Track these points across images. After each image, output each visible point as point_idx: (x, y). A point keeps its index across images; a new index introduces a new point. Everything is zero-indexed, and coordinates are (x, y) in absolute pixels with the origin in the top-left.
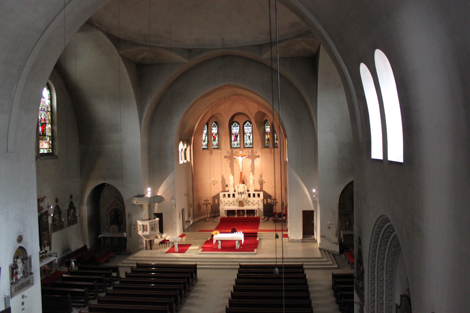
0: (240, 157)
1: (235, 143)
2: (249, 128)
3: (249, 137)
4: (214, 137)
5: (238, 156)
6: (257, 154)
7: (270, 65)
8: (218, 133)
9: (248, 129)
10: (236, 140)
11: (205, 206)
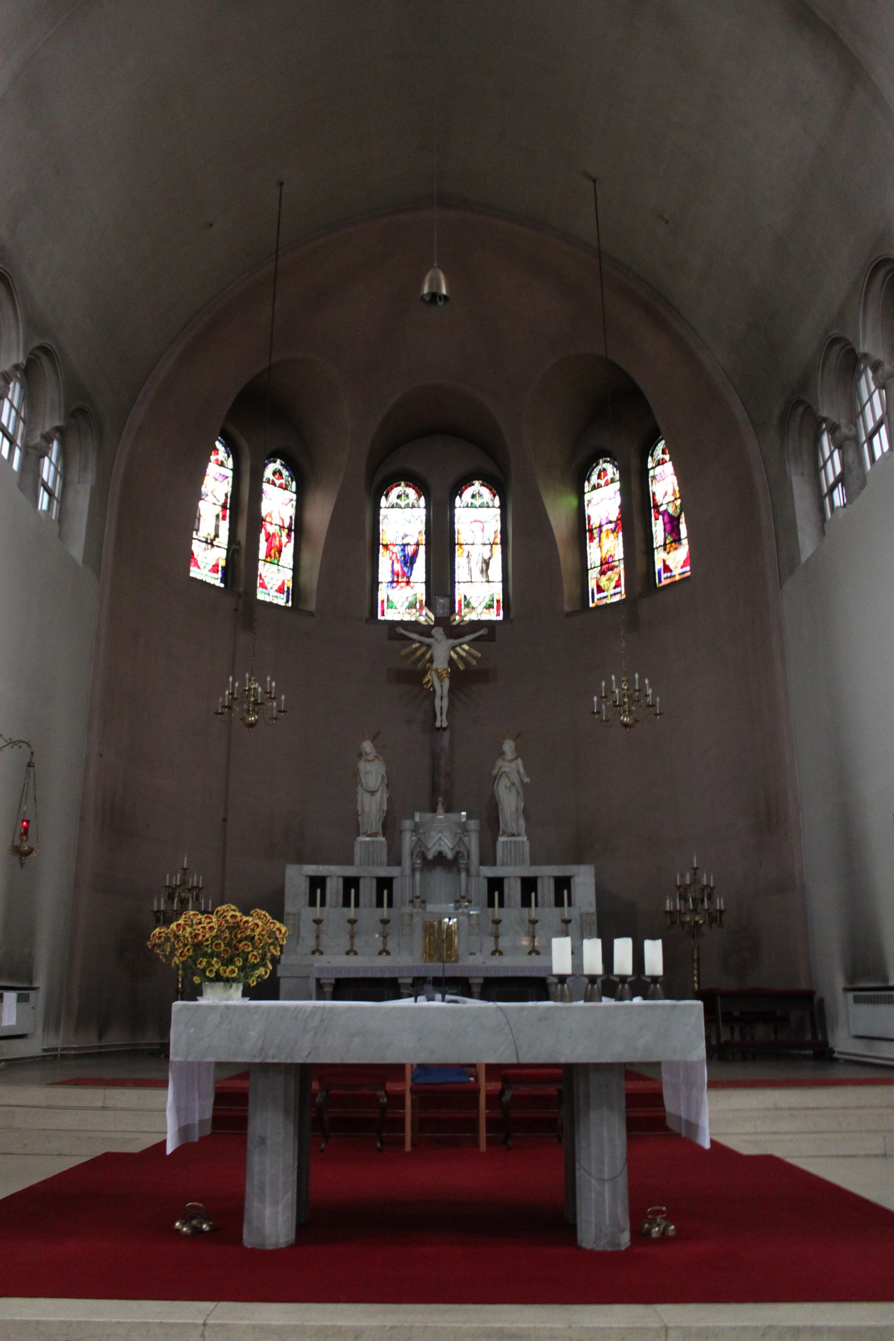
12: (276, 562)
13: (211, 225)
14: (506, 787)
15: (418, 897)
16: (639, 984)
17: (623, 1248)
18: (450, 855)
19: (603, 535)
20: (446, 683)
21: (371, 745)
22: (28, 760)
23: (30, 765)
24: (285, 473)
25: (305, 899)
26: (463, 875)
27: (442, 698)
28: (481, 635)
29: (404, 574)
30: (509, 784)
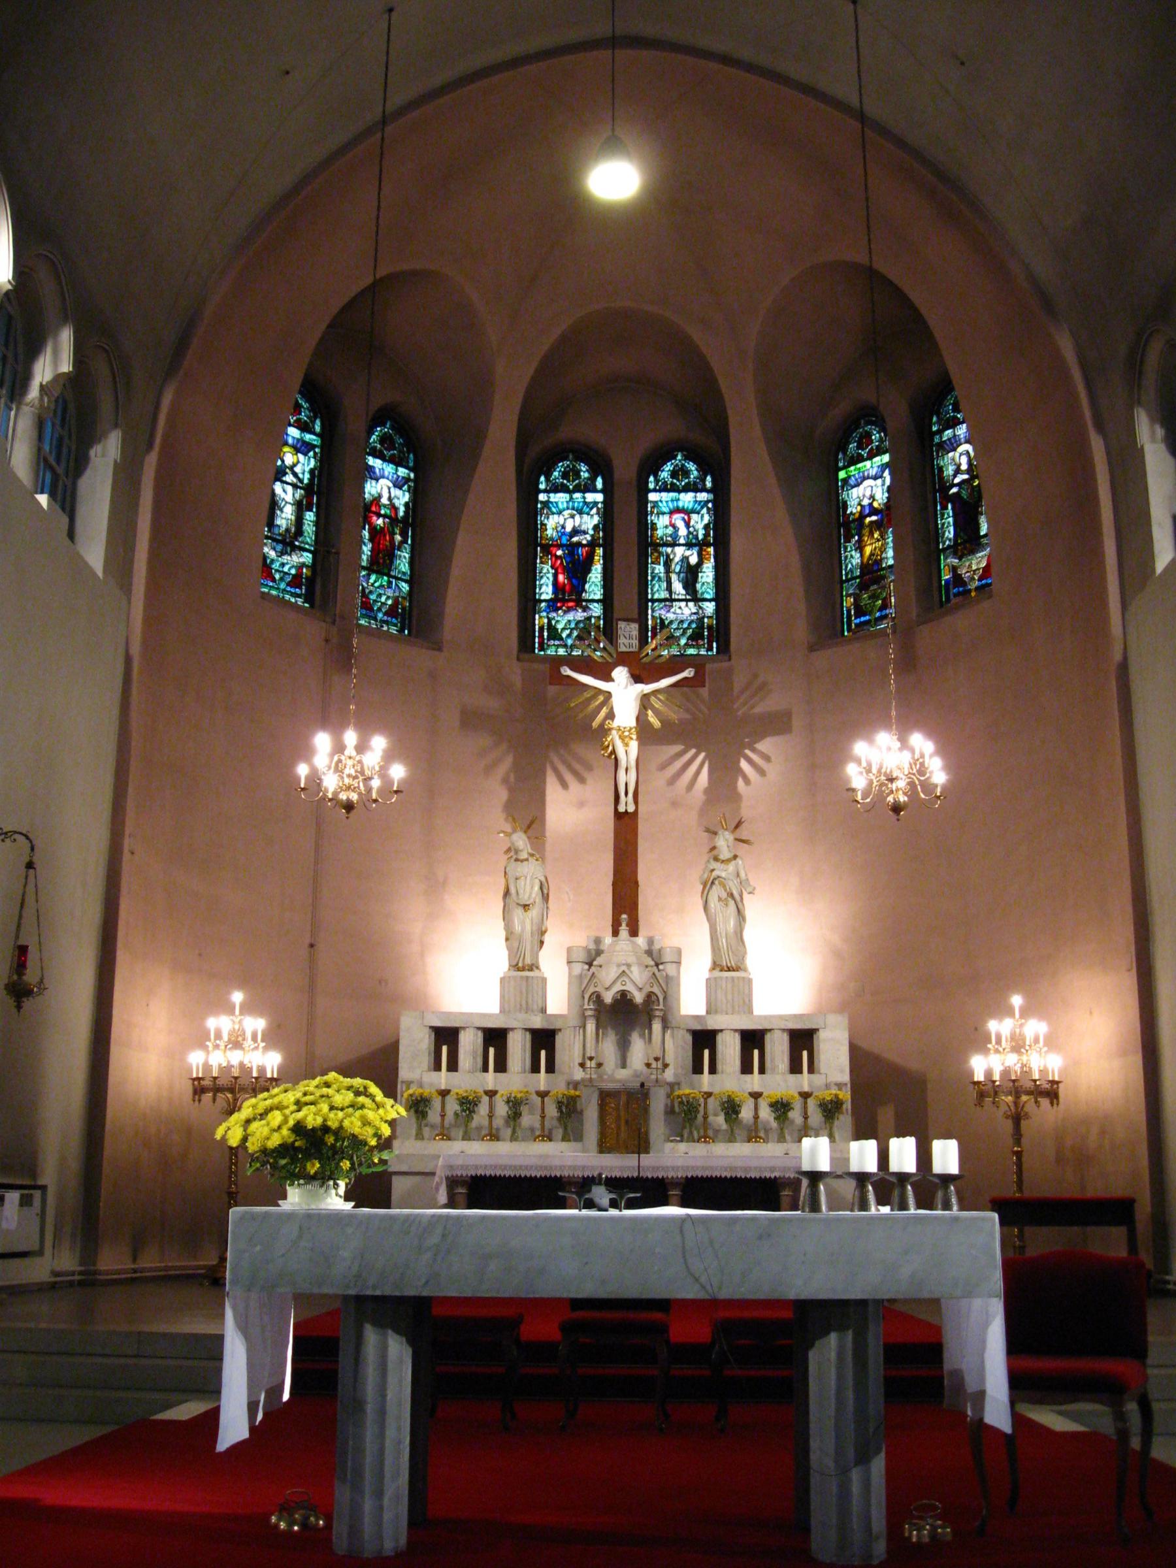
0: (621, 674)
1: (563, 620)
2: (687, 499)
3: (691, 575)
4: (375, 533)
7: (855, 101)
8: (413, 520)
9: (678, 513)
10: (569, 595)
11: (751, 1102)
12: (386, 571)
13: (288, 73)
14: (720, 899)
15: (591, 1059)
16: (928, 1187)
17: (875, 1562)
18: (639, 998)
19: (866, 531)
20: (634, 745)
21: (524, 836)
22: (27, 859)
23: (30, 865)
24: (691, 466)
25: (426, 1060)
26: (657, 1026)
27: (627, 770)
28: (686, 678)
29: (573, 587)
30: (724, 895)
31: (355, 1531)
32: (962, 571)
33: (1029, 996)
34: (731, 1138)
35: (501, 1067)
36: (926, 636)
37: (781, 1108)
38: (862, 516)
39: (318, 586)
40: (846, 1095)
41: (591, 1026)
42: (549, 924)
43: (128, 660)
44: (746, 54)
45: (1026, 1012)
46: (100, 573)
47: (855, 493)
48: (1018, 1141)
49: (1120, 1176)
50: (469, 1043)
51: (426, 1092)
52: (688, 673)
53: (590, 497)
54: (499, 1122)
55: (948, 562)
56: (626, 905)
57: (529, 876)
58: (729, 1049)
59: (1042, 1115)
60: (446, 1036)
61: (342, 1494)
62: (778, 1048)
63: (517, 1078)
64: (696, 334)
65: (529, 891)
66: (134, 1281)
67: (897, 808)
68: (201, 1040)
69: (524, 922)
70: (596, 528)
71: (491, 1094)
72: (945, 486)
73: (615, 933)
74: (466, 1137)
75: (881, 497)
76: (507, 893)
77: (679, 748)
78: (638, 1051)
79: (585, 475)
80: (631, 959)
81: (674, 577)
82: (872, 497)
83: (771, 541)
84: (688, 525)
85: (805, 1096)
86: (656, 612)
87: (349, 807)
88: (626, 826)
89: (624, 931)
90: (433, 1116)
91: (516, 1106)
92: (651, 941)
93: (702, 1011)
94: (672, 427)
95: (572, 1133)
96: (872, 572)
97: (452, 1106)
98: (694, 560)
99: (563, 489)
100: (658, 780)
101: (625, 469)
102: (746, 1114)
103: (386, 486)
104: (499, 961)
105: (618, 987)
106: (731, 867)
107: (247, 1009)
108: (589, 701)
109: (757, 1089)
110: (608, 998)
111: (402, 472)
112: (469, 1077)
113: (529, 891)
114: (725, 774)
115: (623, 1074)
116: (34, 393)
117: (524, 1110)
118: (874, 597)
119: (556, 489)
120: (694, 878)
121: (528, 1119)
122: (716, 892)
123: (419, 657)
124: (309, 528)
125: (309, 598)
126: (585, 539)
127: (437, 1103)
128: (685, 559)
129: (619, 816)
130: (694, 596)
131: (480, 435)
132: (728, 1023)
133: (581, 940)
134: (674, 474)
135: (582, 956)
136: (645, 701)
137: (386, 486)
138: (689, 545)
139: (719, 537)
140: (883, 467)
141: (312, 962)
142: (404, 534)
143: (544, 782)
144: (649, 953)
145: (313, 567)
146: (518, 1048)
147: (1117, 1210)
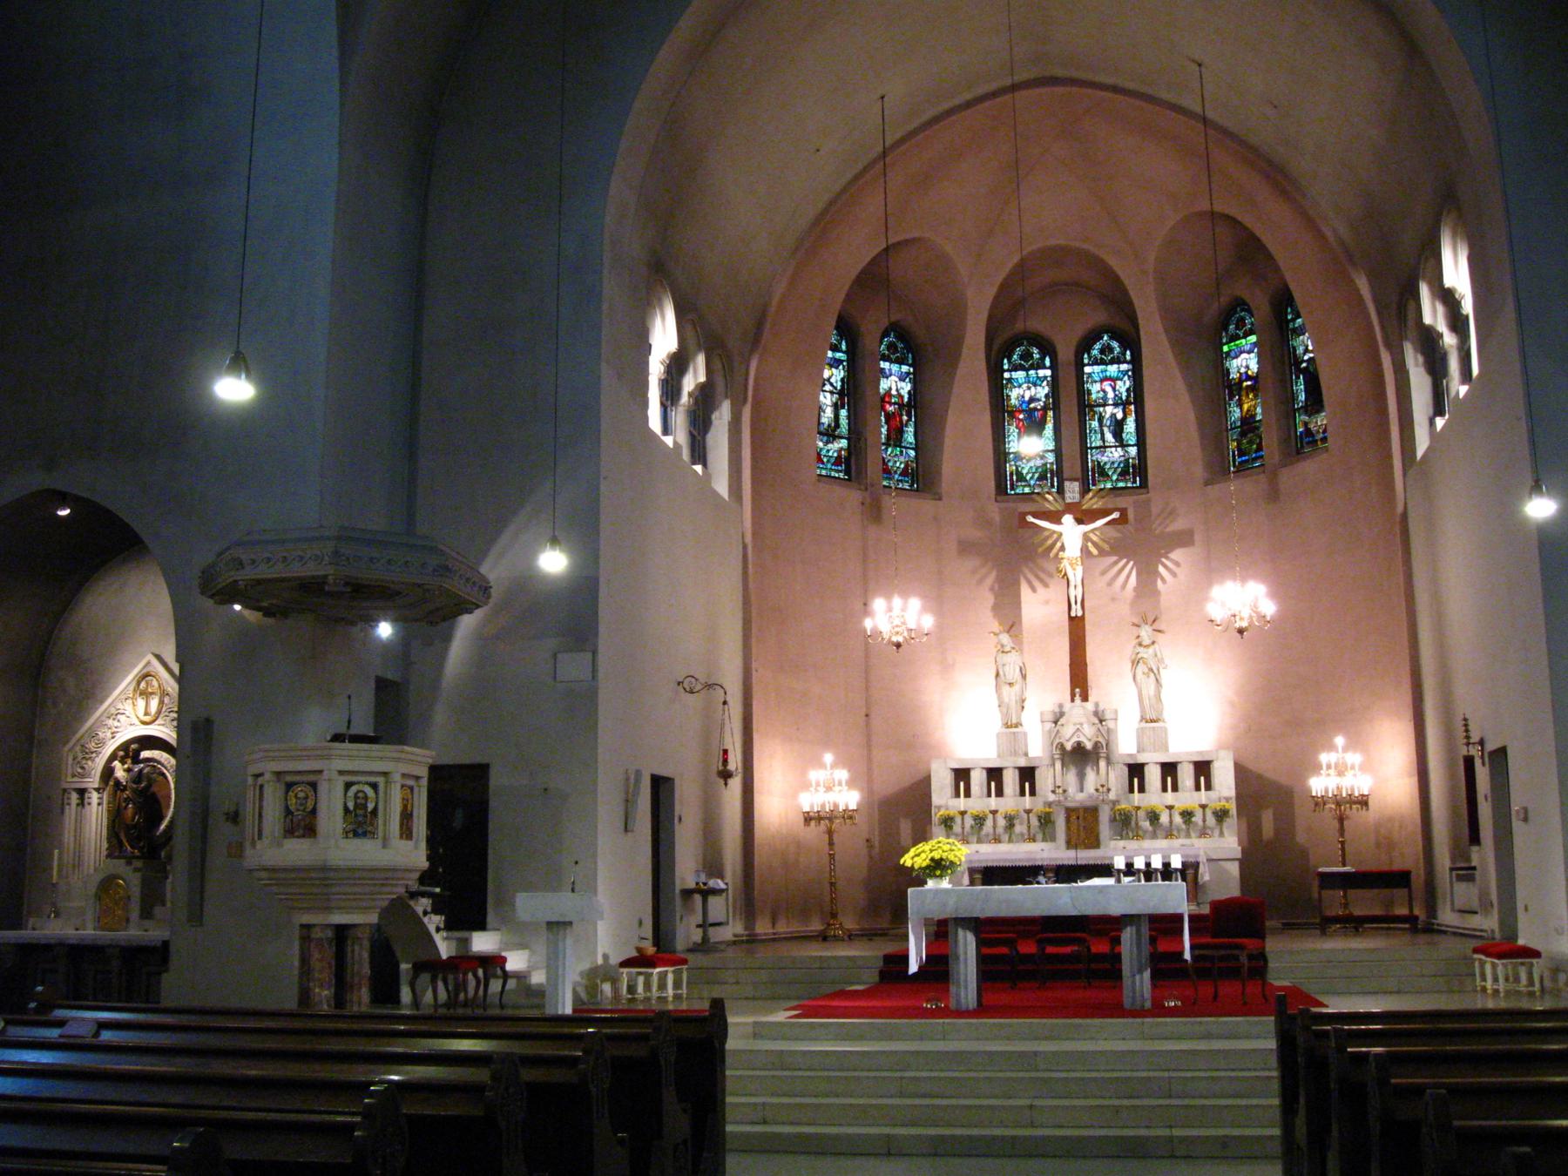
0: (1068, 519)
2: (1112, 370)
4: (889, 417)
5: (1056, 518)
6: (1179, 524)
8: (915, 403)
9: (1107, 381)
18: (1089, 746)
20: (1079, 570)
24: (1115, 344)
25: (949, 790)
26: (1102, 764)
31: (958, 1001)
32: (1311, 426)
33: (1347, 735)
34: (1154, 836)
35: (1000, 793)
36: (1287, 477)
37: (1187, 815)
38: (1241, 381)
39: (851, 463)
40: (1232, 807)
41: (1058, 765)
42: (1027, 695)
43: (745, 547)
44: (1131, 86)
45: (1345, 749)
46: (726, 496)
47: (1235, 363)
48: (1342, 835)
49: (1407, 857)
50: (978, 779)
51: (952, 813)
52: (1115, 515)
53: (1042, 373)
54: (1000, 830)
55: (1301, 418)
56: (1079, 681)
57: (1012, 662)
58: (1153, 775)
59: (1355, 814)
60: (962, 775)
61: (953, 989)
62: (1186, 776)
63: (1011, 801)
64: (1113, 262)
65: (1012, 673)
66: (775, 940)
67: (1241, 631)
68: (806, 786)
69: (1010, 694)
70: (1047, 396)
71: (994, 812)
72: (1298, 362)
73: (1073, 700)
74: (979, 841)
75: (1254, 367)
76: (997, 675)
77: (1115, 558)
78: (1091, 778)
79: (1036, 356)
80: (1083, 720)
81: (1106, 430)
82: (1247, 367)
83: (1174, 406)
84: (1114, 389)
85: (1203, 807)
86: (1092, 457)
87: (898, 645)
88: (1077, 628)
89: (1078, 698)
90: (957, 828)
91: (1011, 821)
92: (1097, 705)
93: (1133, 750)
94: (1099, 317)
95: (1049, 837)
96: (1248, 422)
97: (969, 822)
98: (1120, 416)
99: (1022, 368)
100: (1101, 583)
101: (1066, 353)
102: (1164, 819)
103: (895, 382)
104: (994, 723)
105: (1075, 739)
106: (1151, 650)
107: (834, 766)
108: (1047, 538)
109: (1169, 803)
110: (1069, 747)
111: (905, 368)
112: (979, 801)
113: (1012, 673)
114: (1148, 576)
115: (1080, 797)
116: (685, 399)
117: (1016, 822)
118: (1251, 442)
119: (1015, 368)
120: (1129, 649)
121: (1019, 828)
122: (1141, 668)
123: (926, 506)
124: (844, 422)
125: (847, 472)
126: (1039, 405)
127: (958, 820)
128: (1113, 415)
129: (1071, 619)
130: (1122, 444)
131: (959, 341)
132: (1152, 762)
133: (1050, 706)
134: (1102, 351)
135: (1050, 717)
136: (1086, 537)
137: (895, 382)
138: (1116, 405)
139: (1136, 398)
140: (1255, 344)
141: (868, 724)
142: (909, 415)
143: (1019, 596)
144: (1096, 713)
145: (849, 449)
146: (1010, 780)
147: (1400, 879)
